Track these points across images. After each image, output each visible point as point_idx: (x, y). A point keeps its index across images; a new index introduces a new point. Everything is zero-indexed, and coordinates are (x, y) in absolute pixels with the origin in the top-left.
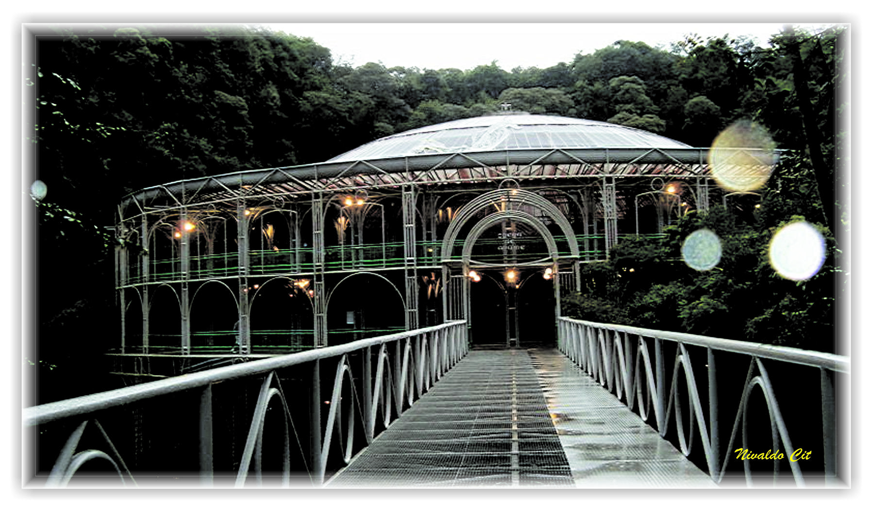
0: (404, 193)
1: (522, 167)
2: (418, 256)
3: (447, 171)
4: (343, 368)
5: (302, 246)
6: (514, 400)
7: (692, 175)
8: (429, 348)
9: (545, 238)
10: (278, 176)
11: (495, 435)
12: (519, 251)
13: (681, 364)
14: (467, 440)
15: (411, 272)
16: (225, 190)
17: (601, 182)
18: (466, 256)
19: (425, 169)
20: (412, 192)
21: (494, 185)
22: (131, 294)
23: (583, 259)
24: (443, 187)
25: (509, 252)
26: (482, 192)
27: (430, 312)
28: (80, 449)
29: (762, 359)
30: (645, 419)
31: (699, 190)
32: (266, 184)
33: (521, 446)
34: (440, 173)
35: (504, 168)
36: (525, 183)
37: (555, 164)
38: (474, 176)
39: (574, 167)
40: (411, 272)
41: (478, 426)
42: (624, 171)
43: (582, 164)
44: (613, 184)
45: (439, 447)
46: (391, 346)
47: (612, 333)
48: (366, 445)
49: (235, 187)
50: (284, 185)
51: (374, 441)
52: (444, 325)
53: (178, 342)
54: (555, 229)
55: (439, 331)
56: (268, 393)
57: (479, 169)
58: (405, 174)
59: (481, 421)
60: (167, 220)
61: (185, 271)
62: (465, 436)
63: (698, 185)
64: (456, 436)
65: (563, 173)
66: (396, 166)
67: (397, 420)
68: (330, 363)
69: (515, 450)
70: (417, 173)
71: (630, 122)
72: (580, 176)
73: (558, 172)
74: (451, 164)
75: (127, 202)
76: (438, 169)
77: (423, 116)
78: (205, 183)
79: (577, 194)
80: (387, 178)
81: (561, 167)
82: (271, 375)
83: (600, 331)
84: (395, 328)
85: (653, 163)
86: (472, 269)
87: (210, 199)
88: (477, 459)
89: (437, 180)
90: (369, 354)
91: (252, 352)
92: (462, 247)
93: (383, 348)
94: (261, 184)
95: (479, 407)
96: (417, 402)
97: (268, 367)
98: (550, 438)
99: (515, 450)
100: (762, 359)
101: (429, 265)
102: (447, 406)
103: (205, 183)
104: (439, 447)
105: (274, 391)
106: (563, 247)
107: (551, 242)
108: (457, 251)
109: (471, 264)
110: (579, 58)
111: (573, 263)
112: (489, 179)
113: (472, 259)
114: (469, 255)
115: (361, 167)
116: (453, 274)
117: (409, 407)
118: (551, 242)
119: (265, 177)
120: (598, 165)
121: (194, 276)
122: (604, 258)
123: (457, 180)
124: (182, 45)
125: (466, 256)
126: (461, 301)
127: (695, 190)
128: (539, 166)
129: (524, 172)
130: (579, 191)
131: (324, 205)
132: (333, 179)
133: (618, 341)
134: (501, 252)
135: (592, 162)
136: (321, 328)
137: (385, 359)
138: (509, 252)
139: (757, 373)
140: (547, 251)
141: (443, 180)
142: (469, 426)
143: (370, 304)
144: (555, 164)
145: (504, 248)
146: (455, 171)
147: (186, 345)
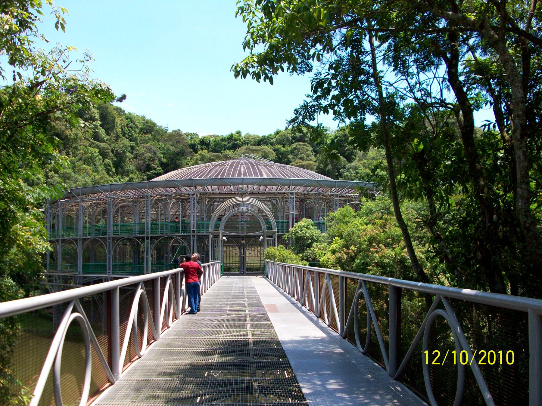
1: (250, 186)
6: (246, 299)
9: (262, 224)
11: (240, 315)
12: (247, 227)
14: (226, 317)
15: (147, 238)
16: (101, 193)
18: (221, 230)
25: (242, 227)
28: (73, 312)
29: (446, 298)
33: (252, 320)
34: (209, 187)
35: (241, 186)
37: (266, 185)
38: (226, 189)
40: (147, 238)
41: (229, 311)
42: (300, 190)
51: (181, 317)
52: (210, 263)
53: (76, 268)
55: (209, 266)
57: (229, 186)
58: (192, 187)
65: (269, 189)
66: (189, 183)
69: (248, 321)
70: (198, 187)
72: (278, 191)
73: (267, 189)
79: (276, 200)
80: (183, 189)
81: (269, 187)
88: (231, 326)
91: (114, 273)
99: (248, 321)
100: (446, 298)
101: (202, 233)
105: (142, 290)
124: (455, 363)
125: (221, 230)
129: (250, 188)
134: (238, 228)
138: (242, 227)
141: (211, 191)
145: (240, 226)
146: (216, 187)
147: (80, 269)
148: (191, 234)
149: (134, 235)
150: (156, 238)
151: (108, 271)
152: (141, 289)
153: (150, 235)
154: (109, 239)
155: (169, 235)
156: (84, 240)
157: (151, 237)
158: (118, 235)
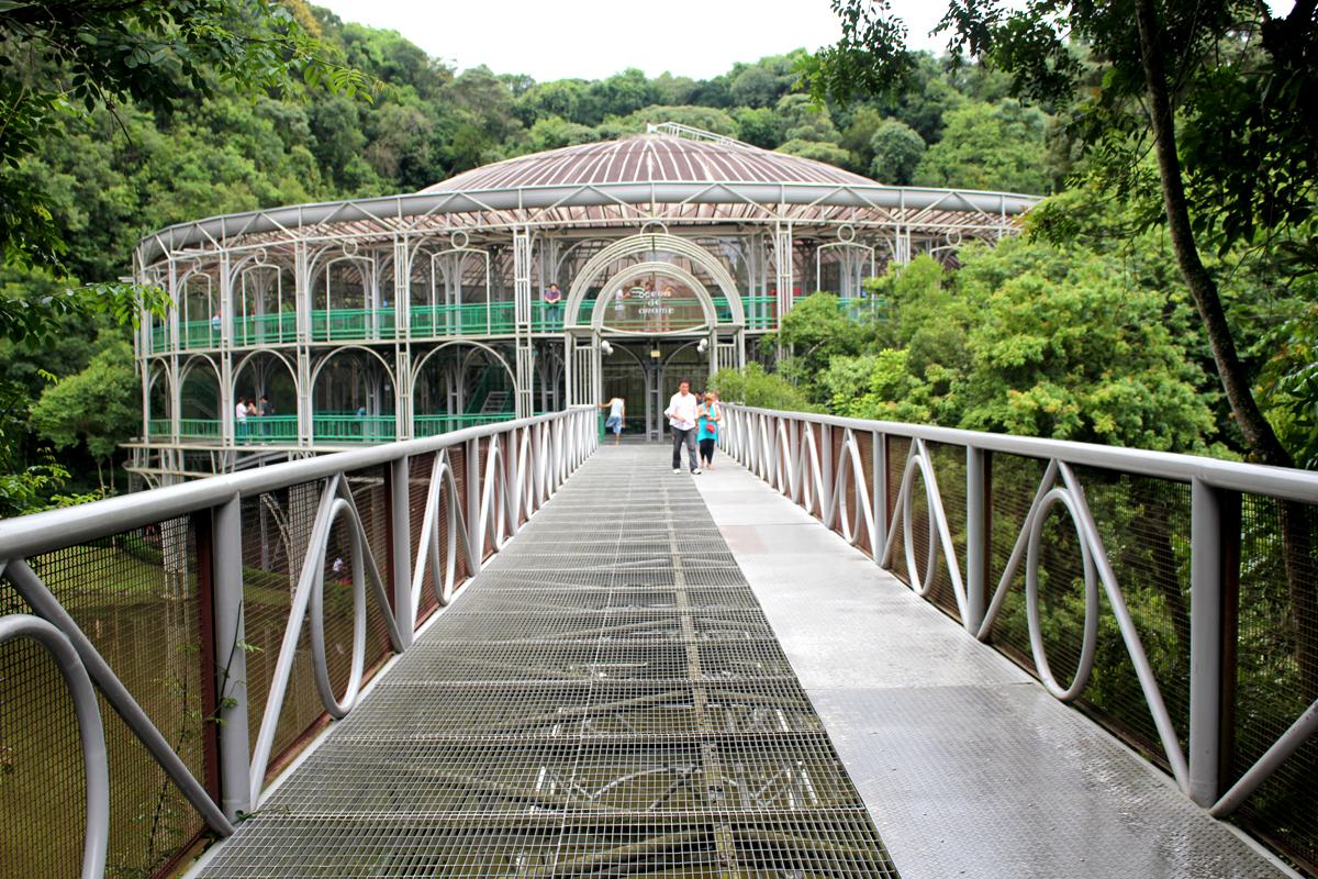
0: (516, 236)
2: (533, 319)
3: (572, 209)
4: (440, 467)
5: (381, 305)
7: (889, 223)
8: (504, 462)
9: (703, 303)
10: (349, 211)
13: (848, 449)
14: (613, 568)
15: (524, 341)
16: (279, 230)
17: (773, 228)
19: (543, 206)
20: (526, 235)
21: (634, 229)
22: (156, 364)
23: (747, 328)
24: (566, 229)
26: (618, 238)
27: (550, 394)
30: (851, 540)
31: (898, 242)
32: (333, 222)
36: (676, 227)
39: (738, 208)
40: (524, 341)
41: (624, 547)
42: (803, 215)
43: (748, 203)
44: (789, 231)
45: (574, 577)
46: (505, 436)
47: (800, 423)
48: (393, 648)
49: (293, 226)
50: (357, 224)
51: (483, 568)
54: (715, 291)
56: (330, 506)
59: (626, 541)
60: (205, 268)
61: (228, 335)
62: (609, 561)
63: (898, 235)
64: (598, 561)
67: (470, 581)
68: (423, 462)
69: (680, 584)
71: (803, 152)
73: (717, 213)
74: (575, 200)
75: (150, 243)
76: (561, 205)
77: (541, 140)
78: (252, 219)
81: (721, 207)
82: (336, 481)
83: (808, 426)
84: (500, 415)
85: (840, 205)
86: (604, 338)
87: (259, 242)
89: (559, 222)
90: (476, 447)
92: (591, 311)
93: (441, 456)
94: (327, 223)
95: (621, 522)
96: (511, 539)
97: (331, 468)
98: (726, 566)
102: (580, 519)
103: (252, 219)
104: (574, 577)
105: (340, 502)
106: (724, 313)
107: (708, 304)
108: (585, 315)
109: (603, 331)
110: (739, 68)
111: (736, 332)
112: (627, 219)
113: (605, 325)
114: (602, 320)
115: (459, 202)
116: (579, 344)
117: (496, 551)
118: (708, 304)
119: (332, 212)
120: (770, 206)
121: (239, 342)
122: (776, 327)
123: (585, 221)
126: (589, 380)
127: (894, 242)
128: (692, 205)
130: (744, 239)
131: (410, 250)
132: (421, 217)
133: (809, 434)
135: (762, 202)
136: (405, 413)
137: (445, 475)
139: (917, 452)
140: (703, 317)
142: (613, 547)
143: (467, 380)
144: (714, 203)
148: (397, 341)
149: (207, 350)
150: (427, 347)
151: (301, 436)
152: (339, 494)
153: (408, 340)
154: (303, 352)
155: (460, 339)
156: (237, 358)
157: (412, 345)
158: (326, 340)
